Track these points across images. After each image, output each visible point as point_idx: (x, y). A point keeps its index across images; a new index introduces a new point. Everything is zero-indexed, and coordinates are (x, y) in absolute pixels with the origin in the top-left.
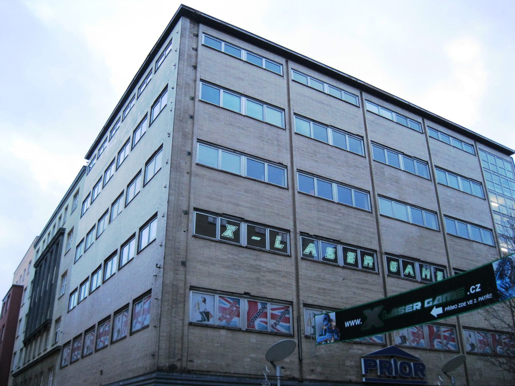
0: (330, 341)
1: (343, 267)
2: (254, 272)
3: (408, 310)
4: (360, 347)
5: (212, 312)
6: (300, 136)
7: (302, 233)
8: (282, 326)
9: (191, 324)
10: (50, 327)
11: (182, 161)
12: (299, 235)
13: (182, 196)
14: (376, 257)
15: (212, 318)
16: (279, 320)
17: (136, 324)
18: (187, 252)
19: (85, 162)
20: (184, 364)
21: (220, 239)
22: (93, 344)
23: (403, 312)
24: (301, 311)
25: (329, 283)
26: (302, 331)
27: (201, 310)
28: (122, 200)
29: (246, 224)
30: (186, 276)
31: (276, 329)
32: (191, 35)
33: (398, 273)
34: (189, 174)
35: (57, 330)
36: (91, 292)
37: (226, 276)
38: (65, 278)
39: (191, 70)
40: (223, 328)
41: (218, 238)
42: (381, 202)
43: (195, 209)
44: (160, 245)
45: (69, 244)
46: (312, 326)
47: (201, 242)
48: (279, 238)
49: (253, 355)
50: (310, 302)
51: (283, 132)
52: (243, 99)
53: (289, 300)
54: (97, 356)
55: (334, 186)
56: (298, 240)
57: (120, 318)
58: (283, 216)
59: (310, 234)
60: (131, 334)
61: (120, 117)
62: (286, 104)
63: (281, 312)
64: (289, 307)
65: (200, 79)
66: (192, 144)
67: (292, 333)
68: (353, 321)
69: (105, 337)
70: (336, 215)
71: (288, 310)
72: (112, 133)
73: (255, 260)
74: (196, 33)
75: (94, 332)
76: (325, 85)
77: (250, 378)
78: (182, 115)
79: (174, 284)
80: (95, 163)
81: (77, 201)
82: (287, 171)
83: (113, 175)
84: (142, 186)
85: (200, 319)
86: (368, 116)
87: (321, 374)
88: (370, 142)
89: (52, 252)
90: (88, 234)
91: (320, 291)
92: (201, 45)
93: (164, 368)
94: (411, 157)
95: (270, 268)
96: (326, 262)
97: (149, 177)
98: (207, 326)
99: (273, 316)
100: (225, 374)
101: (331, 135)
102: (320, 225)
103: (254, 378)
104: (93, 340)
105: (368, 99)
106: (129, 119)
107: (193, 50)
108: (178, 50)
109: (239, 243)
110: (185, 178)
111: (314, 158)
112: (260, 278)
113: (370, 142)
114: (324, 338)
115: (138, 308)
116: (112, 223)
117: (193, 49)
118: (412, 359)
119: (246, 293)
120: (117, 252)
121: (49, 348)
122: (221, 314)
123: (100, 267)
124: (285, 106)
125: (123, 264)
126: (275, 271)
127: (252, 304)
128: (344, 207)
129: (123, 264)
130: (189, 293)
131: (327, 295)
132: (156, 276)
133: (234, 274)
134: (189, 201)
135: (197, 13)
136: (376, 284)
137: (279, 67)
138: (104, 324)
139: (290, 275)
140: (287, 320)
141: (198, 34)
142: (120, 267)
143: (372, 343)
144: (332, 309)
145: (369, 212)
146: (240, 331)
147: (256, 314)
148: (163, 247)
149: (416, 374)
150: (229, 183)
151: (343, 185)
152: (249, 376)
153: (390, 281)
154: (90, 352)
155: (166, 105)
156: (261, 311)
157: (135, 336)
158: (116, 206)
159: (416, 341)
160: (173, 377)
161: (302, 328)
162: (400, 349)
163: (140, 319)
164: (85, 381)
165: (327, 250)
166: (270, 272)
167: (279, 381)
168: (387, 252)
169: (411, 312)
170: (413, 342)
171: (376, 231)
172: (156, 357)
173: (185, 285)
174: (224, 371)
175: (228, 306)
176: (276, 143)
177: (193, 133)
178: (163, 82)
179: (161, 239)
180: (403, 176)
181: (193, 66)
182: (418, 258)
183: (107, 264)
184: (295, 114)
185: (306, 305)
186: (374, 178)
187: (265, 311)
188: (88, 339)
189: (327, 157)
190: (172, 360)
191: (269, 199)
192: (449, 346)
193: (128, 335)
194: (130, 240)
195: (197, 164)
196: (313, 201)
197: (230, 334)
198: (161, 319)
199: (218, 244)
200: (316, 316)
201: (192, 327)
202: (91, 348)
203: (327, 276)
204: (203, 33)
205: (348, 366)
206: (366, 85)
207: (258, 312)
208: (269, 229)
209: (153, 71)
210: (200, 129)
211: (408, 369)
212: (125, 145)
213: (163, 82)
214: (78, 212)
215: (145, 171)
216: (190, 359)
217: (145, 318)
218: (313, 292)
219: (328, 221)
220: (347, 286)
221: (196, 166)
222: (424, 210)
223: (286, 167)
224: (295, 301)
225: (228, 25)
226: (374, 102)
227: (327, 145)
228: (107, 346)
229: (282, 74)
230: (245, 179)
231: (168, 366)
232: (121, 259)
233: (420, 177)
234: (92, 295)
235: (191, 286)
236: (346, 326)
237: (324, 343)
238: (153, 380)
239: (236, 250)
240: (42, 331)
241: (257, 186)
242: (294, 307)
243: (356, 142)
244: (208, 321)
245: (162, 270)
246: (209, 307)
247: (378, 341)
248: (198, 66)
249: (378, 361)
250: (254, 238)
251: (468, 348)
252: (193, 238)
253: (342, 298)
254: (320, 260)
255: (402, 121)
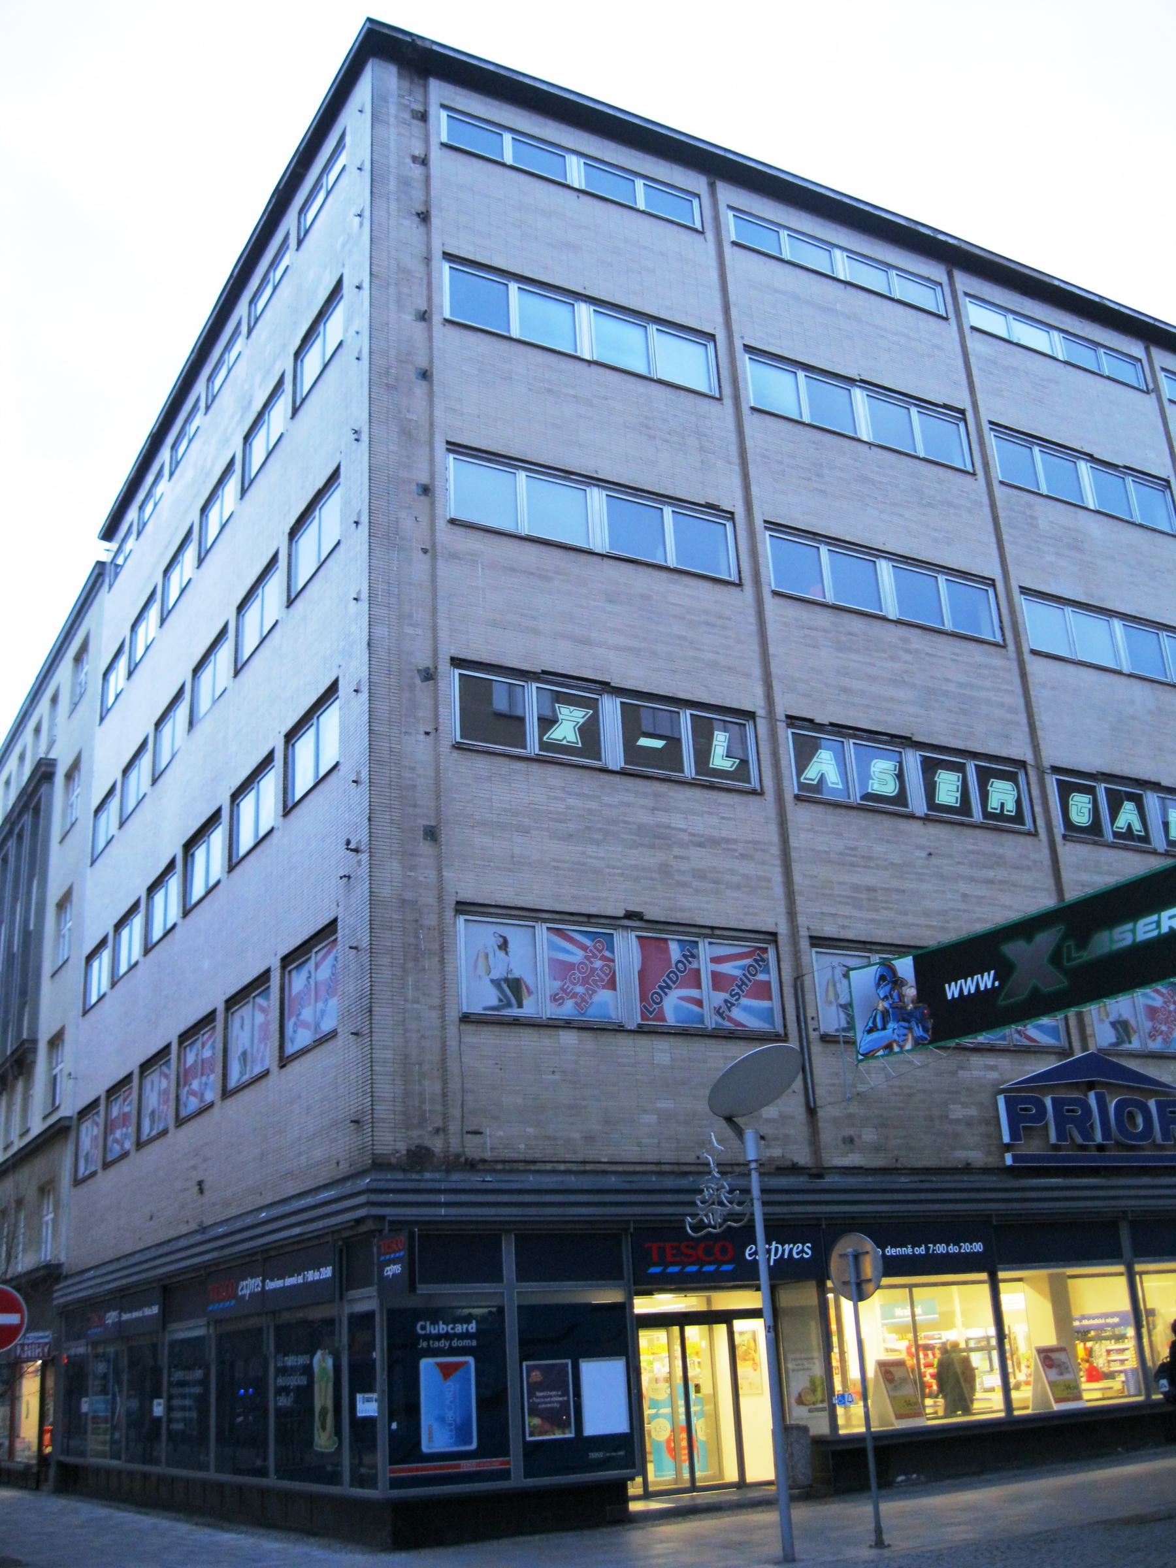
0: (901, 1047)
1: (926, 819)
2: (652, 846)
3: (1145, 933)
4: (991, 1060)
5: (529, 979)
7: (792, 720)
8: (747, 1009)
9: (466, 1019)
10: (34, 1062)
11: (403, 514)
13: (411, 625)
14: (1025, 781)
15: (533, 997)
16: (737, 990)
17: (295, 1032)
18: (438, 797)
19: (103, 551)
20: (455, 1145)
21: (540, 750)
22: (167, 1101)
23: (1128, 941)
24: (805, 959)
25: (886, 868)
26: (809, 1019)
27: (496, 975)
28: (225, 654)
29: (619, 700)
30: (440, 870)
31: (731, 1020)
33: (1095, 828)
34: (429, 554)
35: (55, 1072)
36: (149, 946)
37: (566, 865)
38: (68, 910)
39: (411, 226)
40: (567, 1025)
41: (533, 747)
42: (1029, 610)
43: (457, 662)
44: (354, 781)
45: (71, 806)
46: (841, 1006)
47: (481, 764)
48: (720, 741)
49: (662, 1105)
50: (830, 930)
51: (714, 407)
52: (583, 309)
53: (764, 929)
54: (181, 1138)
55: (885, 568)
56: (781, 740)
57: (245, 1018)
58: (730, 669)
59: (818, 720)
60: (284, 1061)
61: (198, 400)
62: (719, 318)
63: (743, 968)
64: (765, 950)
65: (444, 253)
66: (432, 461)
67: (781, 1031)
68: (969, 979)
69: (204, 1079)
70: (893, 658)
71: (763, 960)
72: (177, 451)
73: (654, 809)
74: (421, 109)
75: (169, 1068)
76: (837, 253)
78: (393, 371)
79: (407, 898)
80: (131, 551)
81: (86, 674)
82: (735, 527)
83: (190, 580)
84: (285, 604)
86: (976, 344)
87: (877, 1149)
88: (986, 427)
89: (20, 837)
90: (126, 771)
92: (438, 146)
93: (394, 1160)
94: (1115, 466)
95: (701, 833)
96: (873, 804)
97: (303, 574)
98: (516, 1023)
99: (719, 981)
100: (582, 1168)
101: (864, 409)
102: (845, 690)
103: (672, 1173)
104: (166, 1092)
105: (972, 292)
106: (226, 401)
107: (414, 162)
108: (367, 167)
109: (600, 759)
110: (420, 566)
111: (816, 485)
112: (671, 866)
113: (986, 427)
114: (882, 1038)
115: (298, 982)
116: (199, 729)
117: (414, 159)
118: (1151, 1090)
119: (630, 915)
120: (220, 817)
121: (37, 1127)
122: (557, 984)
123: (171, 866)
124: (712, 323)
125: (243, 851)
126: (714, 842)
127: (652, 947)
128: (918, 631)
129: (242, 851)
130: (455, 924)
131: (883, 908)
132: (349, 877)
133: (590, 857)
134: (435, 639)
135: (419, 43)
137: (688, 204)
138: (196, 1040)
139: (763, 851)
140: (763, 991)
141: (426, 111)
142: (235, 860)
143: (1029, 1047)
144: (901, 949)
145: (996, 645)
146: (623, 1031)
147: (665, 977)
148: (364, 787)
151: (912, 565)
153: (1070, 853)
154: (161, 1127)
155: (340, 344)
156: (680, 965)
157: (295, 1067)
158: (206, 675)
160: (423, 1185)
161: (810, 1012)
162: (1115, 1060)
163: (307, 1014)
164: (151, 1218)
165: (873, 769)
167: (755, 1175)
168: (1058, 764)
169: (1155, 937)
170: (1152, 1036)
171: (1021, 702)
172: (367, 1128)
173: (440, 899)
174: (580, 1157)
175: (577, 956)
176: (692, 441)
177: (432, 424)
178: (327, 272)
179: (357, 761)
180: (1096, 528)
181: (418, 215)
182: (1153, 779)
183: (193, 855)
184: (748, 348)
185: (818, 941)
186: (1005, 537)
187: (694, 966)
188: (152, 1088)
189: (856, 480)
190: (414, 1133)
191: (684, 618)
193: (274, 1068)
194: (258, 776)
195: (453, 522)
196: (823, 618)
197: (588, 1041)
198: (374, 1009)
199: (535, 768)
200: (852, 973)
202: (163, 1115)
203: (879, 849)
204: (444, 107)
205: (958, 1121)
206: (964, 246)
207: (672, 972)
208: (688, 712)
209: (293, 241)
210: (454, 410)
211: (1140, 1120)
212: (221, 482)
213: (327, 272)
214: (90, 707)
215: (290, 556)
216: (471, 1129)
217: (323, 1012)
218: (838, 899)
219: (873, 679)
220: (942, 877)
221: (450, 526)
222: (1166, 630)
223: (731, 516)
224: (783, 930)
225: (521, 79)
227: (854, 443)
228: (211, 1105)
229: (698, 226)
230: (605, 560)
231: (404, 1152)
232: (235, 836)
233: (1147, 528)
234: (151, 955)
235: (458, 903)
236: (949, 997)
237: (881, 1053)
238: (362, 1199)
239: (589, 783)
240: (10, 1078)
241: (641, 580)
243: (944, 428)
244: (520, 1006)
245: (364, 857)
246: (518, 963)
247: (1045, 1040)
248: (434, 213)
249: (1048, 1101)
250: (644, 742)
253: (927, 914)
254: (852, 800)
255: (1084, 357)
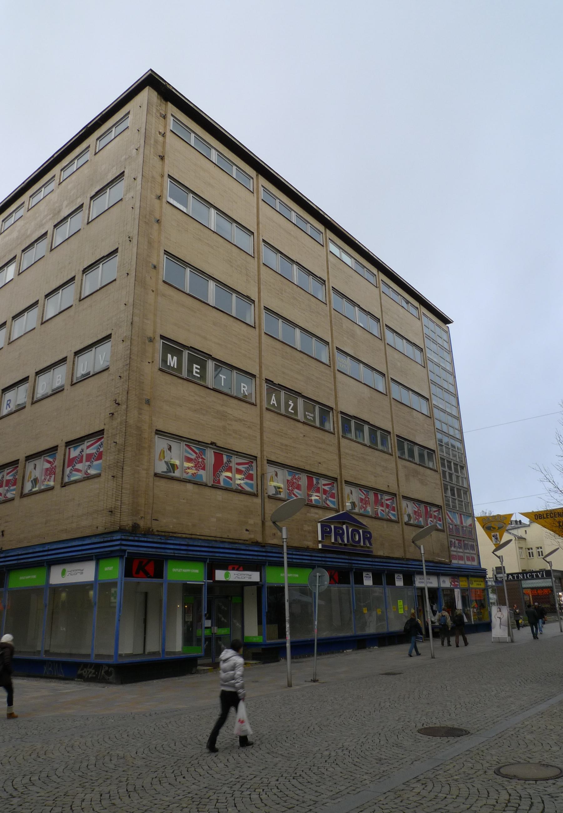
6: (268, 268)
9: (156, 475)
12: (264, 382)
25: (291, 439)
29: (214, 362)
32: (157, 114)
40: (189, 481)
43: (162, 337)
49: (219, 515)
50: (273, 458)
71: (252, 466)
73: (222, 405)
77: (216, 541)
78: (148, 217)
85: (165, 470)
91: (282, 447)
94: (365, 311)
119: (212, 443)
127: (310, 479)
128: (306, 356)
133: (201, 419)
135: (168, 86)
136: (332, 444)
147: (221, 468)
149: (364, 543)
150: (198, 312)
152: (214, 539)
159: (364, 507)
166: (236, 421)
192: (328, 502)
196: (279, 345)
201: (157, 479)
216: (154, 518)
223: (253, 302)
226: (336, 243)
242: (258, 462)
249: (333, 527)
251: (406, 519)
252: (160, 372)
